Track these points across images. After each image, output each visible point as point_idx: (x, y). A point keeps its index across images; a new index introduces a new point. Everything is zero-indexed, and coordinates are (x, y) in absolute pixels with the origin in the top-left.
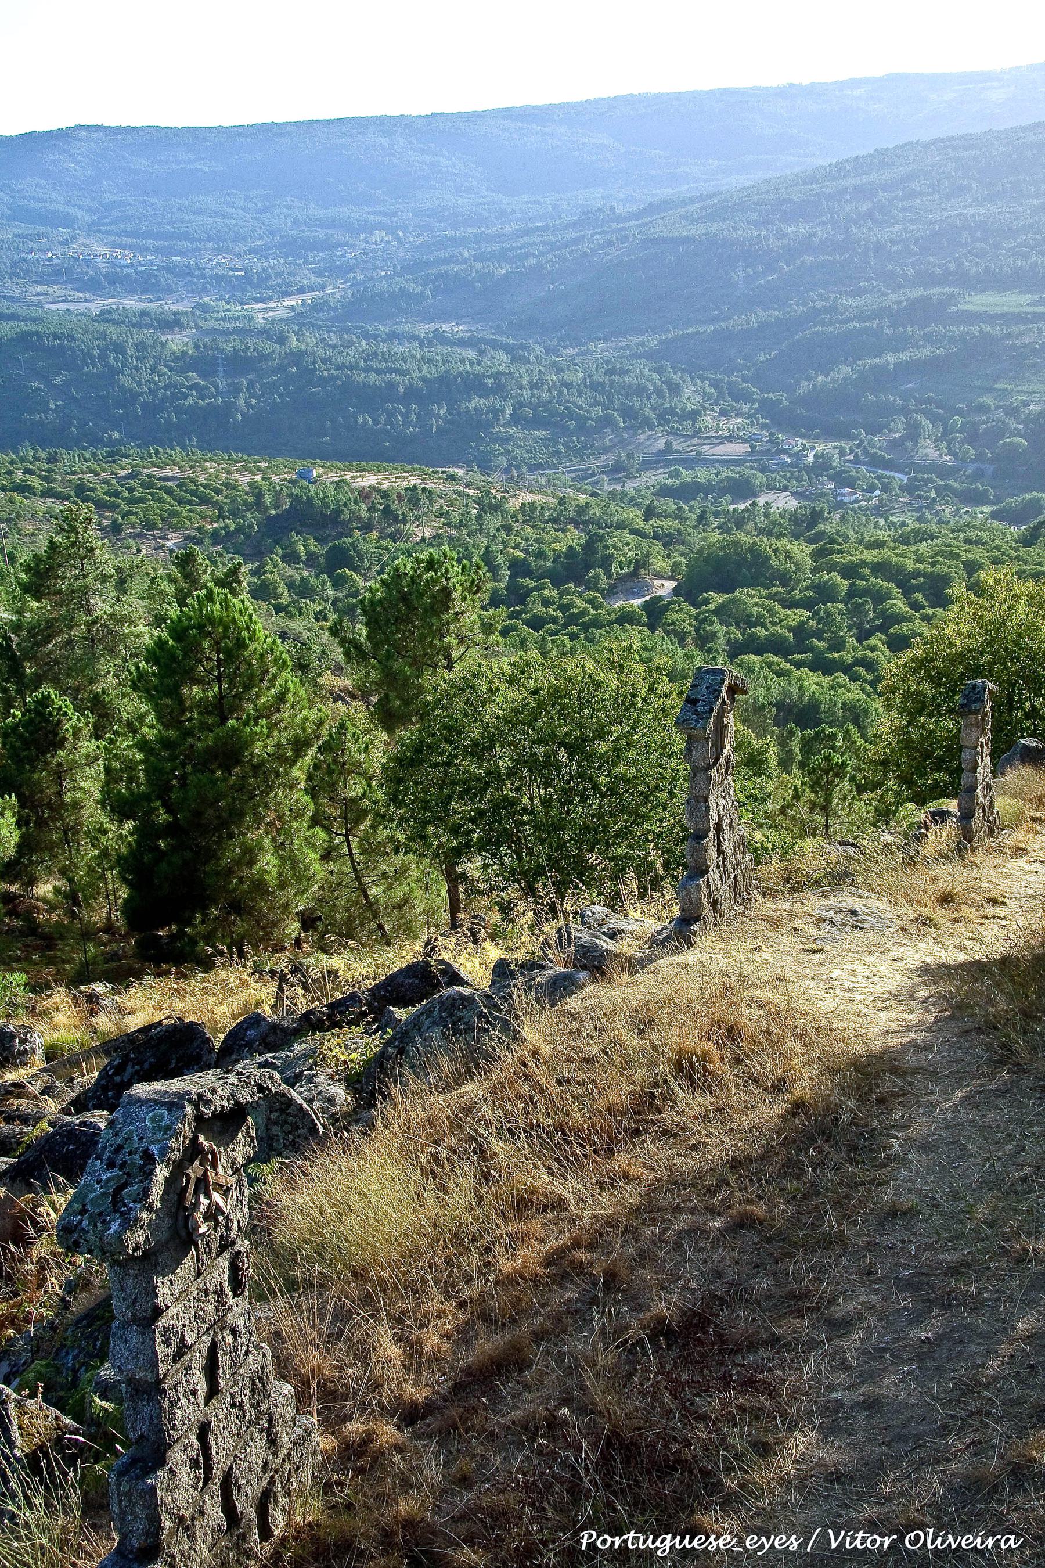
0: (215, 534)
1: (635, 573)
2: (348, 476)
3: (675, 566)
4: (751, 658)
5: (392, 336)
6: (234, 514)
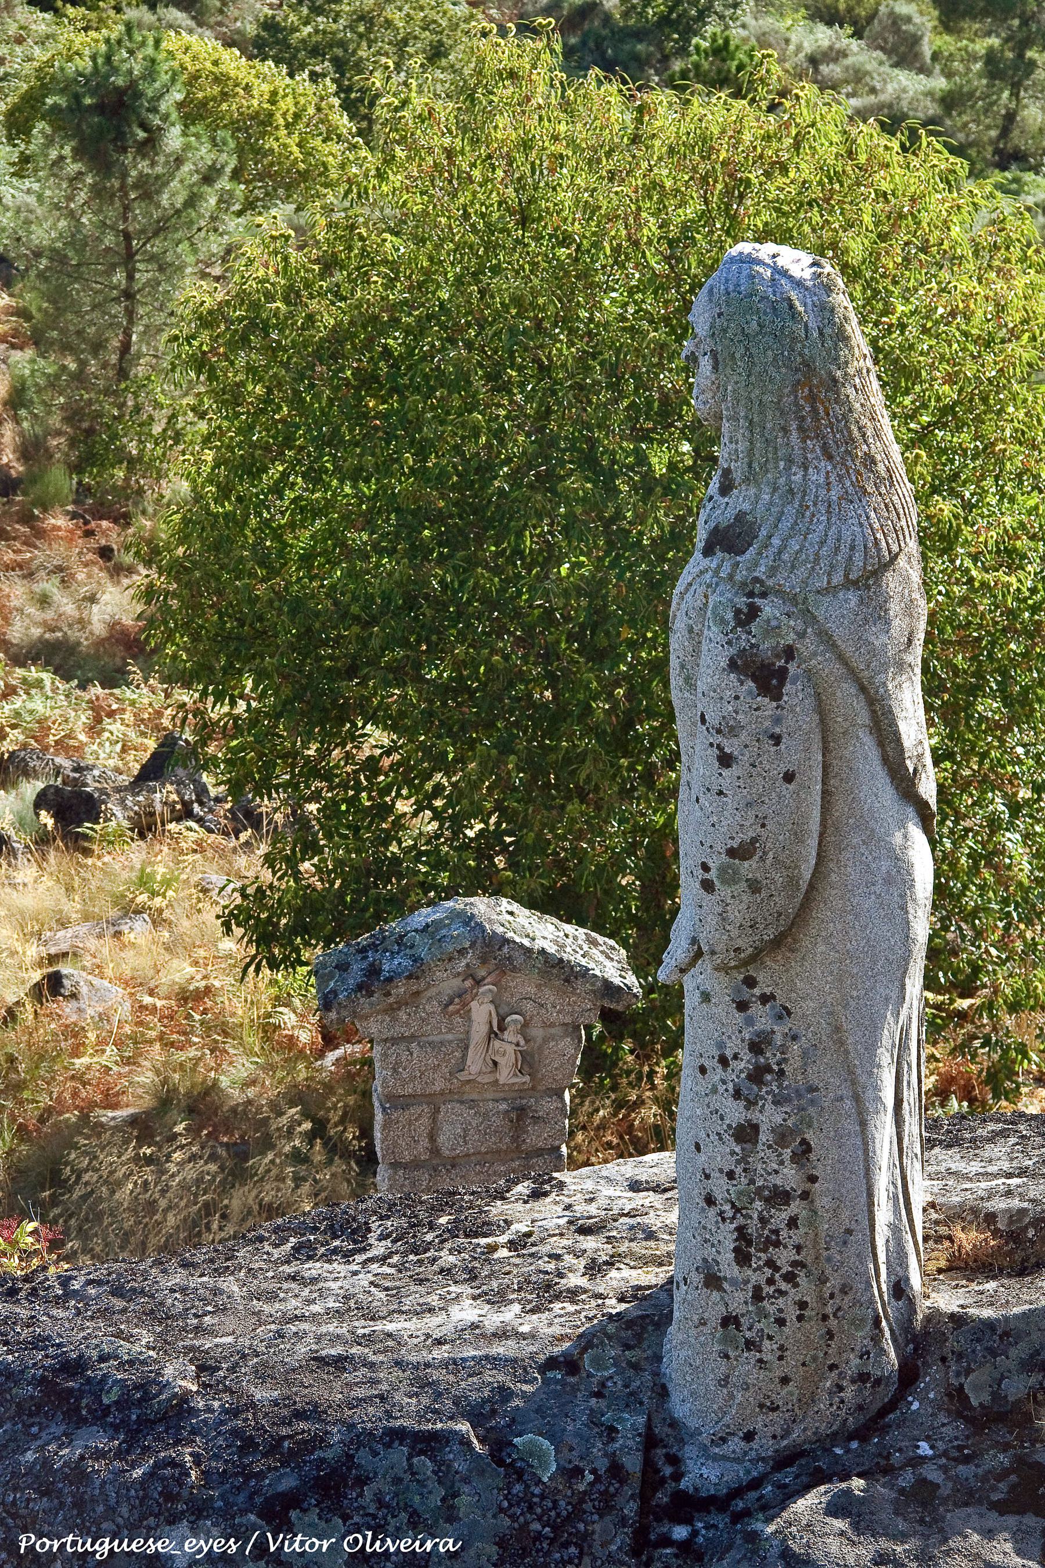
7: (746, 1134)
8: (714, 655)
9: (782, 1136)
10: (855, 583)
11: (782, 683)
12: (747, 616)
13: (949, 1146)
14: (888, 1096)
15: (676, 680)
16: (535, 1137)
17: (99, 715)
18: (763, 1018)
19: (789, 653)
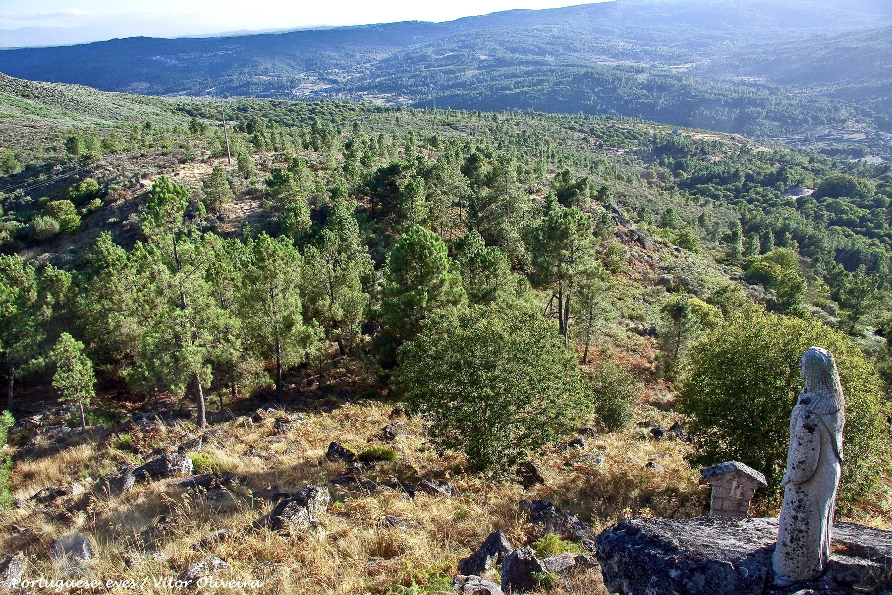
0: (636, 151)
1: (797, 185)
2: (691, 134)
3: (815, 185)
4: (837, 227)
5: (724, 81)
6: (645, 145)
7: (795, 518)
8: (800, 423)
9: (803, 519)
12: (808, 417)
13: (621, 483)
14: (826, 515)
15: (791, 427)
16: (742, 509)
17: (664, 417)
18: (802, 496)
19: (816, 425)
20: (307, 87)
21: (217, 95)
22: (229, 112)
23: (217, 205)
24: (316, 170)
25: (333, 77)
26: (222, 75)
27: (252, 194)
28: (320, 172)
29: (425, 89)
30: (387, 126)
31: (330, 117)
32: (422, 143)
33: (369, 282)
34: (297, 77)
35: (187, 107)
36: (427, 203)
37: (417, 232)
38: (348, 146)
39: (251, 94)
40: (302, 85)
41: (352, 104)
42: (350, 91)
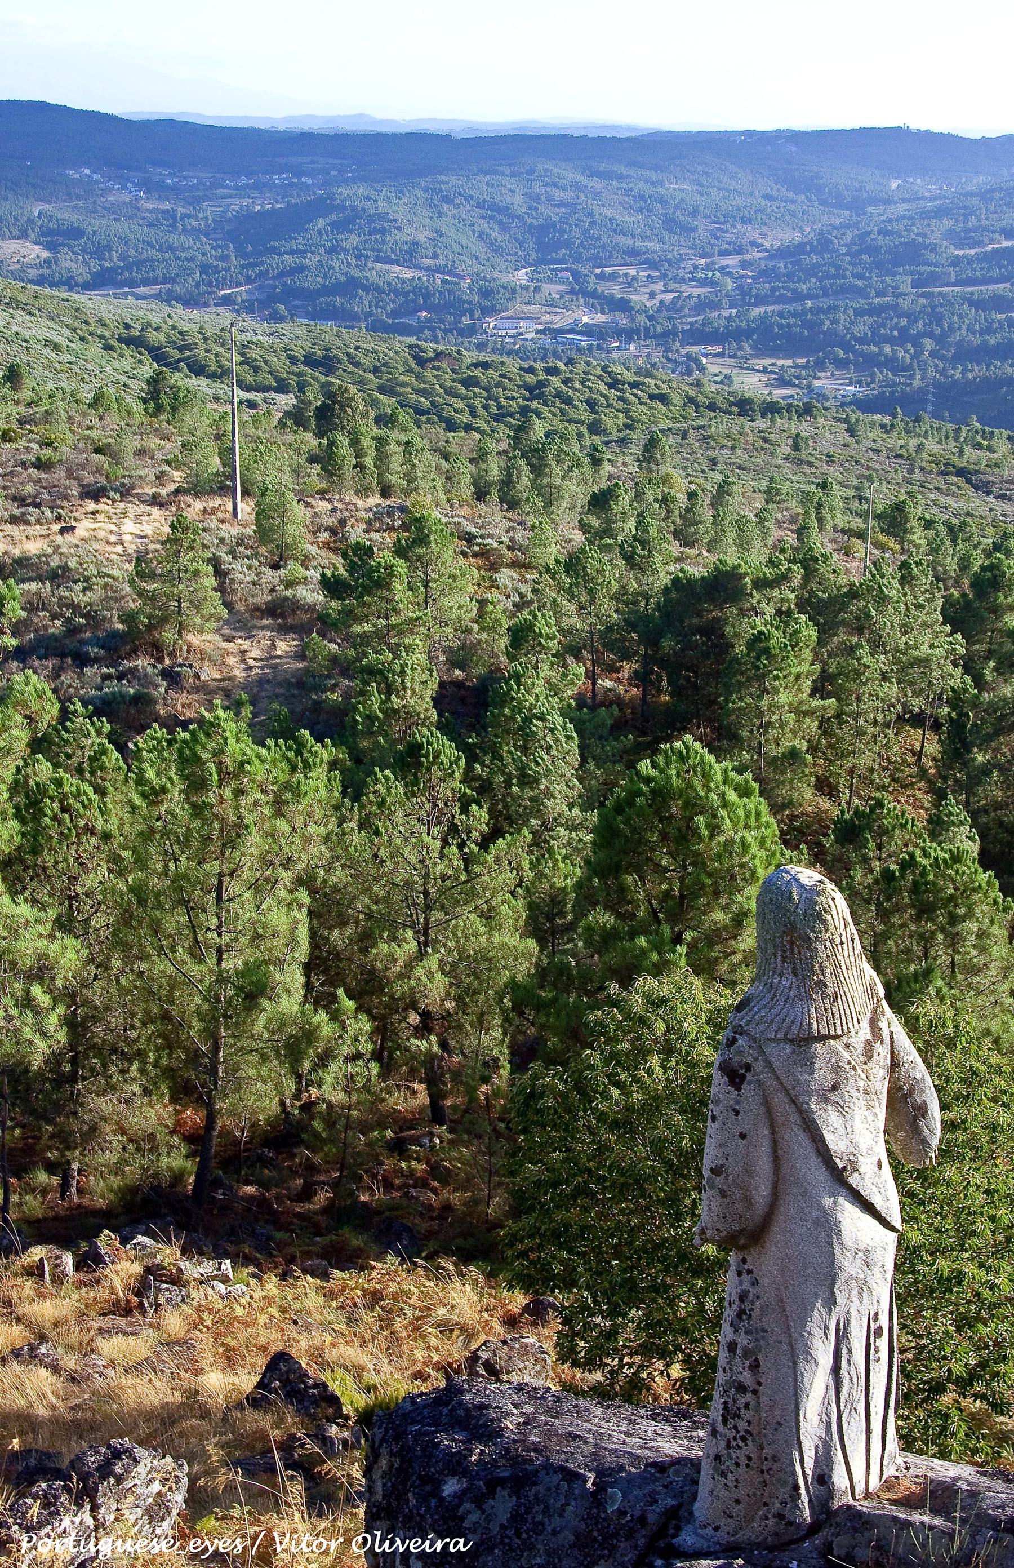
9: (747, 1353)
10: (792, 1041)
11: (742, 1082)
19: (748, 1067)
20: (535, 313)
21: (250, 310)
22: (280, 364)
23: (168, 635)
24: (494, 567)
25: (617, 291)
26: (274, 250)
27: (281, 613)
28: (506, 576)
29: (903, 354)
30: (760, 459)
31: (586, 416)
32: (857, 523)
33: (562, 914)
34: (504, 279)
35: (155, 338)
36: (815, 703)
37: (683, 758)
38: (601, 501)
39: (355, 317)
40: (518, 306)
41: (666, 379)
42: (664, 338)
